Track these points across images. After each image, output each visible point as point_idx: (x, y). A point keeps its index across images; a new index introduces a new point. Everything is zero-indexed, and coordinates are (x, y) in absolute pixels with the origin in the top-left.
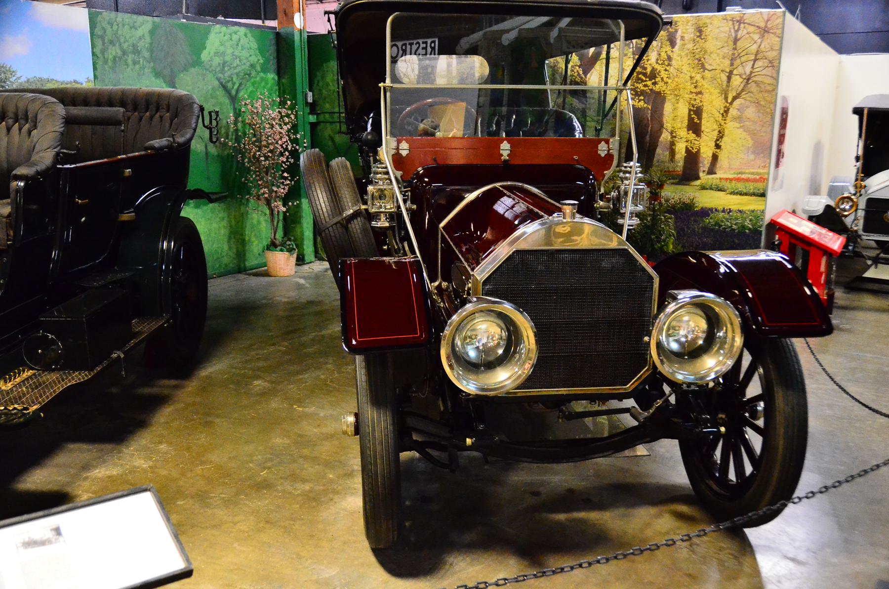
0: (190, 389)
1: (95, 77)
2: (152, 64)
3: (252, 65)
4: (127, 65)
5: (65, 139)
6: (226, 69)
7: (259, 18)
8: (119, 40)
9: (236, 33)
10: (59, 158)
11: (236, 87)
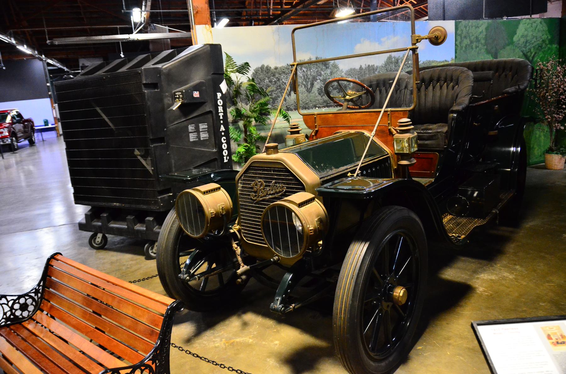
0: (521, 234)
1: (456, 57)
2: (485, 47)
3: (543, 41)
4: (472, 48)
5: (474, 91)
6: (527, 44)
7: (528, 15)
8: (469, 36)
9: (535, 22)
10: (472, 100)
11: (532, 55)
